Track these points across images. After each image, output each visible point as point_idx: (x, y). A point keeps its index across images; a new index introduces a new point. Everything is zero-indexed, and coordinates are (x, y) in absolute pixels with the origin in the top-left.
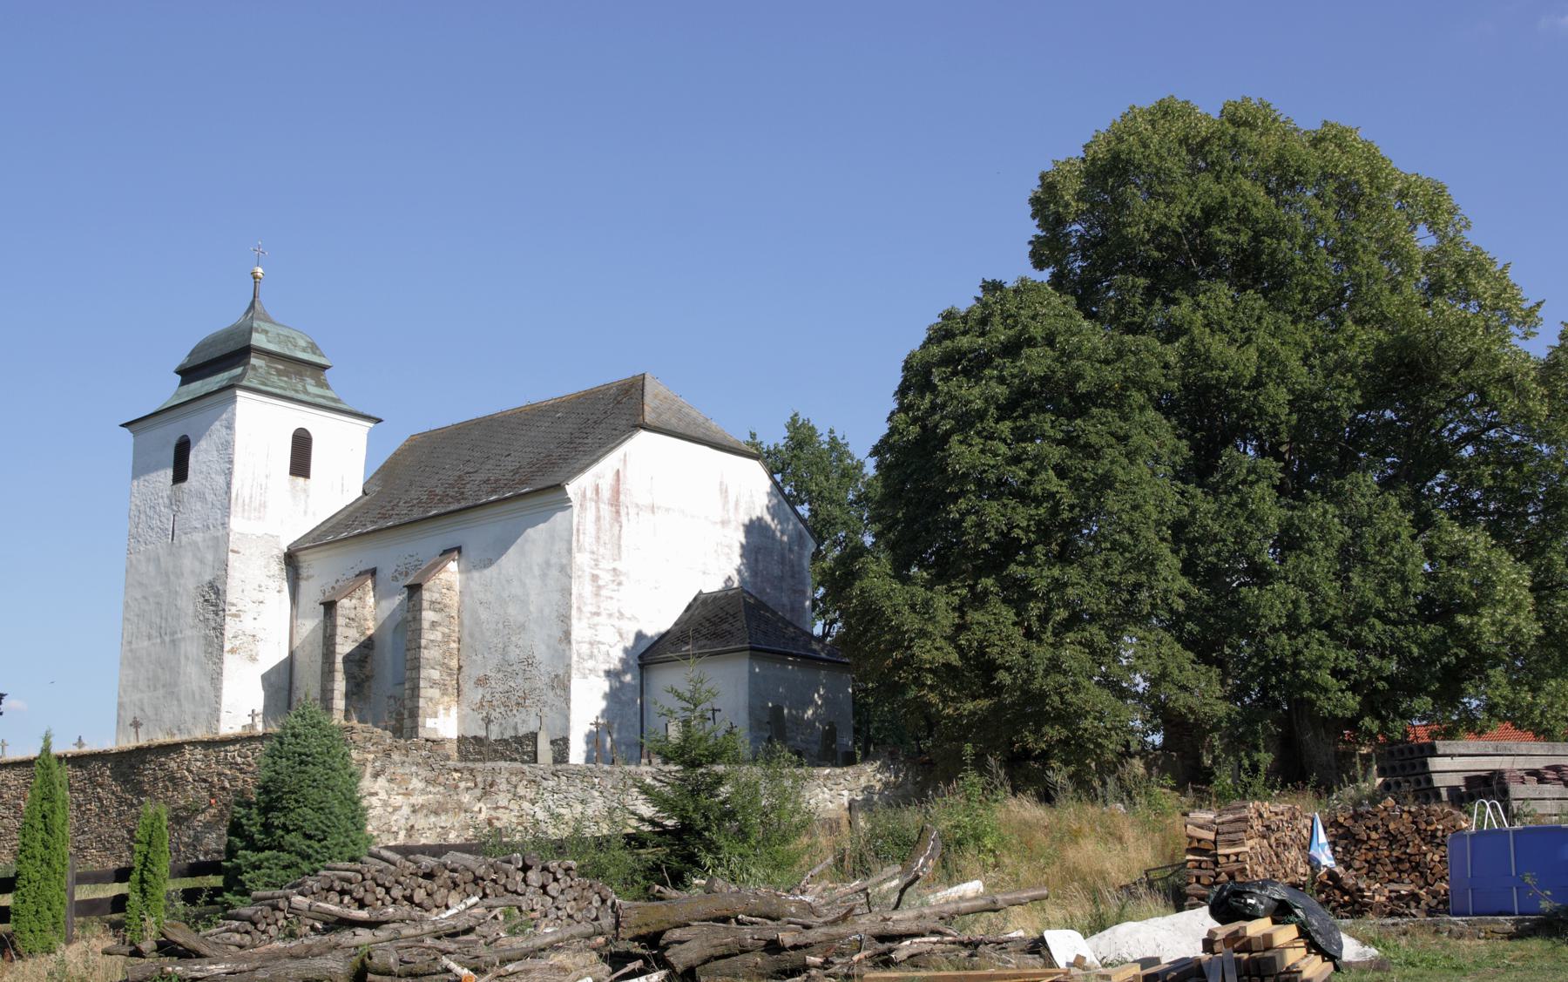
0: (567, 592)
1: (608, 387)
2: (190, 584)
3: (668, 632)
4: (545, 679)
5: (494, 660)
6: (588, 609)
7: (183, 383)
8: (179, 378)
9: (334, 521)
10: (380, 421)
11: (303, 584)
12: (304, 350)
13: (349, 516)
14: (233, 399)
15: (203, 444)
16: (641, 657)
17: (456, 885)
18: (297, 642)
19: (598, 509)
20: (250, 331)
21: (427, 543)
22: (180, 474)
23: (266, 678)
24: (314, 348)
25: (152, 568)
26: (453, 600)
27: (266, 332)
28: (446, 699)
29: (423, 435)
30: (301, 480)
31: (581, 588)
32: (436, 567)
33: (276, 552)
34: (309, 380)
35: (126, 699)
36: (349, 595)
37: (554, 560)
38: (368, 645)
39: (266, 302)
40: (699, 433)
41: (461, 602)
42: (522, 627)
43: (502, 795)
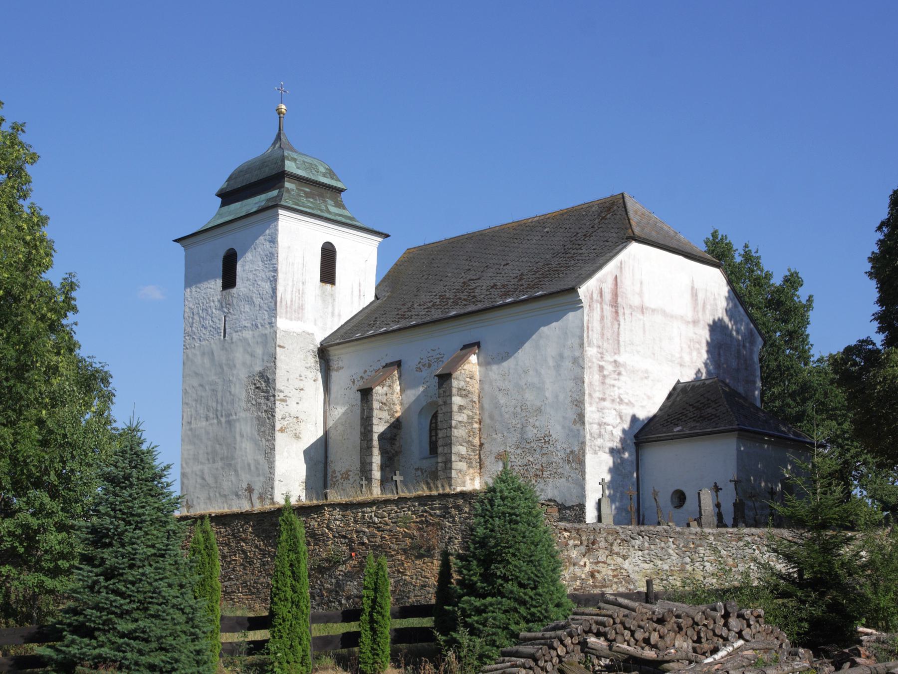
0: (579, 381)
1: (590, 205)
2: (242, 374)
3: (655, 416)
4: (561, 454)
5: (513, 438)
6: (597, 395)
7: (223, 204)
8: (220, 200)
9: (355, 321)
10: (387, 236)
11: (334, 375)
12: (324, 175)
13: (368, 317)
14: (276, 218)
15: (249, 256)
16: (636, 436)
17: (680, 628)
18: (331, 423)
19: (602, 309)
20: (283, 159)
21: (447, 340)
22: (229, 281)
23: (307, 453)
24: (331, 174)
25: (207, 361)
26: (475, 387)
27: (294, 160)
28: (471, 471)
29: (420, 248)
30: (328, 286)
31: (591, 377)
32: (460, 359)
33: (312, 347)
34: (330, 202)
35: (188, 470)
36: (381, 384)
37: (567, 353)
38: (396, 426)
39: (289, 135)
40: (674, 245)
41: (482, 389)
42: (539, 410)
43: (601, 551)
